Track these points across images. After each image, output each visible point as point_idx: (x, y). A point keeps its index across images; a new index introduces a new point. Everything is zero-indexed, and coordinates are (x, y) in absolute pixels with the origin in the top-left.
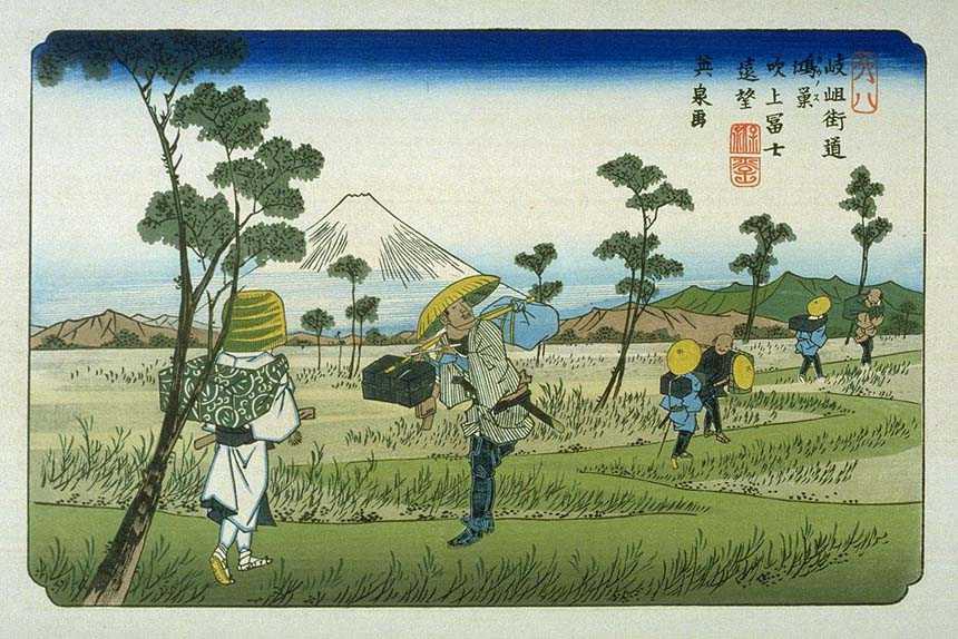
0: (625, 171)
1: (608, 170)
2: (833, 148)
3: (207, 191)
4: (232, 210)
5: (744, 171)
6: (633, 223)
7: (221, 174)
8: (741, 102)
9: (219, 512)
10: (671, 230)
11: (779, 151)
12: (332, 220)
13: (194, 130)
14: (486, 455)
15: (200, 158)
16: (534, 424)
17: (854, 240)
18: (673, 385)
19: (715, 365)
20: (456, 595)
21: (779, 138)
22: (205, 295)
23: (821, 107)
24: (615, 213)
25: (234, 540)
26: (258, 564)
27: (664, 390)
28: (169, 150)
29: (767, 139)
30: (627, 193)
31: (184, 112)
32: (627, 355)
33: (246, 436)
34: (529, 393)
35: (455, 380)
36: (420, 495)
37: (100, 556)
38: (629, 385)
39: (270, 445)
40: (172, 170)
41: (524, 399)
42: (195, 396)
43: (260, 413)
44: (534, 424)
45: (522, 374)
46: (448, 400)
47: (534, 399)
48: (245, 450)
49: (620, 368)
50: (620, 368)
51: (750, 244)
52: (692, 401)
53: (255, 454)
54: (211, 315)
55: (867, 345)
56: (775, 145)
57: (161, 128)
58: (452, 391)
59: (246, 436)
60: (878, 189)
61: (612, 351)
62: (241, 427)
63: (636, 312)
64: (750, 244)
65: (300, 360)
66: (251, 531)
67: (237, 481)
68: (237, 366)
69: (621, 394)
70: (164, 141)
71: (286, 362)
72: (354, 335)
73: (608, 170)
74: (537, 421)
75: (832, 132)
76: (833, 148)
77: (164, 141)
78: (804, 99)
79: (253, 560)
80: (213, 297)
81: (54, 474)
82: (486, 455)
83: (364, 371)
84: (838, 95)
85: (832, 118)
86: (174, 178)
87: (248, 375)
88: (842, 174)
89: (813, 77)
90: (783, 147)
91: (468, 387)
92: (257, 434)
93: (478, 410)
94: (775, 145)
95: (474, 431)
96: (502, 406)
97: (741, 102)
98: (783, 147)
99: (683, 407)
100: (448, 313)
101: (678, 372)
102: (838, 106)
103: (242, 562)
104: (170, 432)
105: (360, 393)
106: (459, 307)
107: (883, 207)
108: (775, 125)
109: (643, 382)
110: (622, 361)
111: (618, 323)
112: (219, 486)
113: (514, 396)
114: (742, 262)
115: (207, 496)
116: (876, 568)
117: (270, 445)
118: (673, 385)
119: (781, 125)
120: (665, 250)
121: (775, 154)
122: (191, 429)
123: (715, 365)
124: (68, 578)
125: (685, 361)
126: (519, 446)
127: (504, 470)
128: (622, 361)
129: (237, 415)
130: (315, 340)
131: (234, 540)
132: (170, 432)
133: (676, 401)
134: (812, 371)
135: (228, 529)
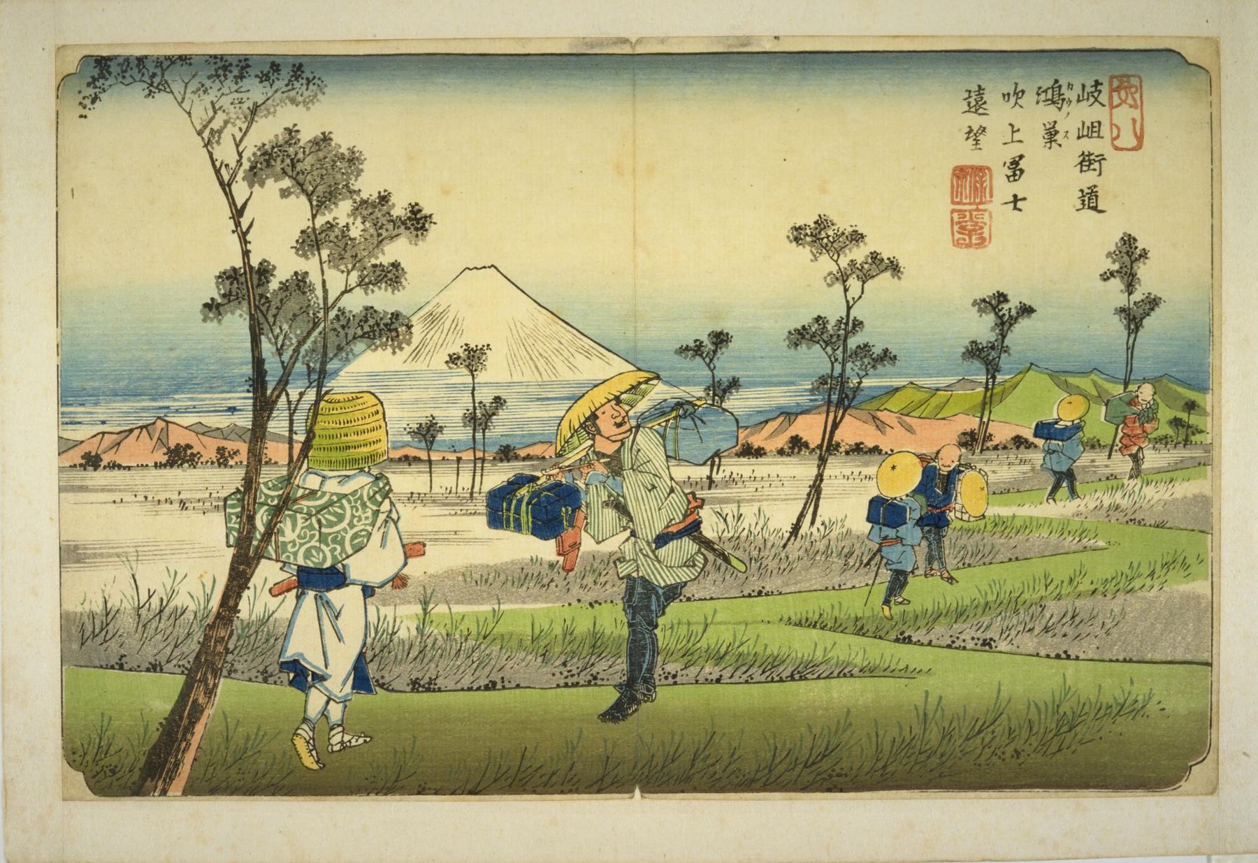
0: (816, 236)
2: (1090, 200)
3: (286, 265)
4: (319, 292)
5: (969, 232)
6: (831, 305)
8: (971, 141)
9: (301, 676)
10: (883, 311)
11: (1020, 204)
12: (444, 300)
13: (273, 186)
14: (645, 601)
15: (279, 220)
18: (884, 512)
19: (937, 486)
20: (596, 787)
21: (1018, 188)
23: (1072, 148)
24: (807, 286)
25: (324, 714)
26: (354, 743)
29: (1002, 189)
31: (265, 164)
32: (240, 473)
36: (573, 657)
39: (368, 591)
41: (692, 529)
42: (270, 531)
43: (358, 549)
45: (690, 497)
46: (600, 536)
47: (708, 531)
48: (334, 596)
49: (816, 489)
50: (816, 489)
51: (982, 328)
52: (911, 533)
53: (346, 598)
54: (291, 422)
55: (1136, 458)
56: (1015, 196)
57: (226, 187)
60: (1144, 255)
61: (804, 469)
62: (333, 567)
63: (836, 417)
64: (982, 328)
65: (403, 482)
66: (344, 701)
68: (325, 489)
69: (818, 521)
70: (232, 203)
71: (388, 483)
73: (798, 235)
74: (711, 557)
75: (1089, 178)
76: (1090, 200)
78: (1051, 134)
79: (347, 738)
80: (568, 404)
84: (1093, 130)
85: (1087, 161)
87: (339, 500)
89: (1060, 109)
90: (1024, 199)
91: (621, 508)
92: (353, 574)
94: (1015, 196)
98: (1024, 199)
99: (899, 540)
100: (597, 417)
101: (889, 494)
104: (239, 578)
105: (484, 519)
107: (1149, 278)
108: (1016, 168)
109: (847, 508)
110: (820, 477)
112: (303, 644)
113: (682, 526)
114: (974, 351)
115: (289, 654)
117: (368, 591)
118: (884, 512)
119: (1022, 171)
120: (874, 335)
121: (1015, 208)
122: (267, 572)
123: (937, 486)
125: (901, 482)
126: (687, 591)
127: (673, 622)
128: (820, 477)
130: (423, 455)
131: (324, 714)
132: (239, 578)
133: (890, 532)
134: (1064, 490)
135: (316, 700)
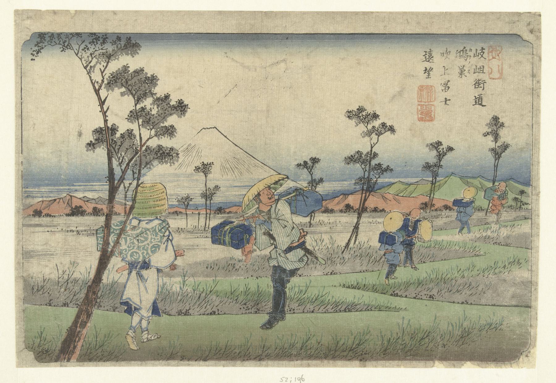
0: (359, 115)
1: (350, 115)
3: (123, 126)
6: (364, 145)
7: (134, 116)
8: (426, 74)
14: (281, 277)
15: (120, 104)
16: (308, 259)
17: (77, 218)
18: (386, 238)
19: (410, 228)
21: (448, 95)
22: (122, 185)
23: (471, 78)
24: (355, 139)
27: (380, 241)
28: (102, 103)
30: (362, 128)
33: (146, 265)
34: (304, 243)
35: (264, 234)
36: (252, 303)
37: (92, 276)
38: (362, 237)
40: (104, 114)
44: (308, 259)
46: (260, 247)
49: (356, 228)
50: (356, 228)
52: (399, 248)
56: (446, 99)
57: (97, 92)
58: (263, 239)
59: (146, 265)
64: (431, 156)
67: (141, 292)
70: (99, 98)
72: (206, 209)
73: (350, 115)
76: (479, 101)
77: (99, 98)
81: (33, 293)
82: (281, 277)
83: (212, 228)
85: (478, 84)
86: (106, 121)
88: (484, 115)
90: (449, 100)
93: (277, 251)
94: (446, 99)
95: (274, 263)
96: (290, 249)
97: (426, 74)
98: (449, 100)
102: (481, 76)
103: (143, 337)
106: (266, 192)
108: (446, 86)
111: (354, 200)
113: (297, 244)
116: (506, 347)
117: (159, 270)
118: (386, 238)
119: (449, 88)
121: (446, 104)
122: (115, 262)
123: (410, 228)
124: (44, 350)
129: (141, 255)
134: (465, 230)
135: (136, 319)
